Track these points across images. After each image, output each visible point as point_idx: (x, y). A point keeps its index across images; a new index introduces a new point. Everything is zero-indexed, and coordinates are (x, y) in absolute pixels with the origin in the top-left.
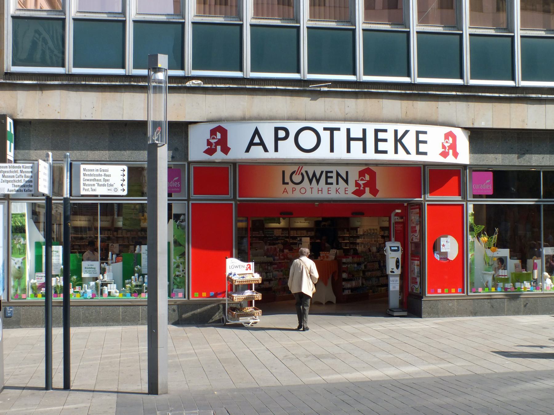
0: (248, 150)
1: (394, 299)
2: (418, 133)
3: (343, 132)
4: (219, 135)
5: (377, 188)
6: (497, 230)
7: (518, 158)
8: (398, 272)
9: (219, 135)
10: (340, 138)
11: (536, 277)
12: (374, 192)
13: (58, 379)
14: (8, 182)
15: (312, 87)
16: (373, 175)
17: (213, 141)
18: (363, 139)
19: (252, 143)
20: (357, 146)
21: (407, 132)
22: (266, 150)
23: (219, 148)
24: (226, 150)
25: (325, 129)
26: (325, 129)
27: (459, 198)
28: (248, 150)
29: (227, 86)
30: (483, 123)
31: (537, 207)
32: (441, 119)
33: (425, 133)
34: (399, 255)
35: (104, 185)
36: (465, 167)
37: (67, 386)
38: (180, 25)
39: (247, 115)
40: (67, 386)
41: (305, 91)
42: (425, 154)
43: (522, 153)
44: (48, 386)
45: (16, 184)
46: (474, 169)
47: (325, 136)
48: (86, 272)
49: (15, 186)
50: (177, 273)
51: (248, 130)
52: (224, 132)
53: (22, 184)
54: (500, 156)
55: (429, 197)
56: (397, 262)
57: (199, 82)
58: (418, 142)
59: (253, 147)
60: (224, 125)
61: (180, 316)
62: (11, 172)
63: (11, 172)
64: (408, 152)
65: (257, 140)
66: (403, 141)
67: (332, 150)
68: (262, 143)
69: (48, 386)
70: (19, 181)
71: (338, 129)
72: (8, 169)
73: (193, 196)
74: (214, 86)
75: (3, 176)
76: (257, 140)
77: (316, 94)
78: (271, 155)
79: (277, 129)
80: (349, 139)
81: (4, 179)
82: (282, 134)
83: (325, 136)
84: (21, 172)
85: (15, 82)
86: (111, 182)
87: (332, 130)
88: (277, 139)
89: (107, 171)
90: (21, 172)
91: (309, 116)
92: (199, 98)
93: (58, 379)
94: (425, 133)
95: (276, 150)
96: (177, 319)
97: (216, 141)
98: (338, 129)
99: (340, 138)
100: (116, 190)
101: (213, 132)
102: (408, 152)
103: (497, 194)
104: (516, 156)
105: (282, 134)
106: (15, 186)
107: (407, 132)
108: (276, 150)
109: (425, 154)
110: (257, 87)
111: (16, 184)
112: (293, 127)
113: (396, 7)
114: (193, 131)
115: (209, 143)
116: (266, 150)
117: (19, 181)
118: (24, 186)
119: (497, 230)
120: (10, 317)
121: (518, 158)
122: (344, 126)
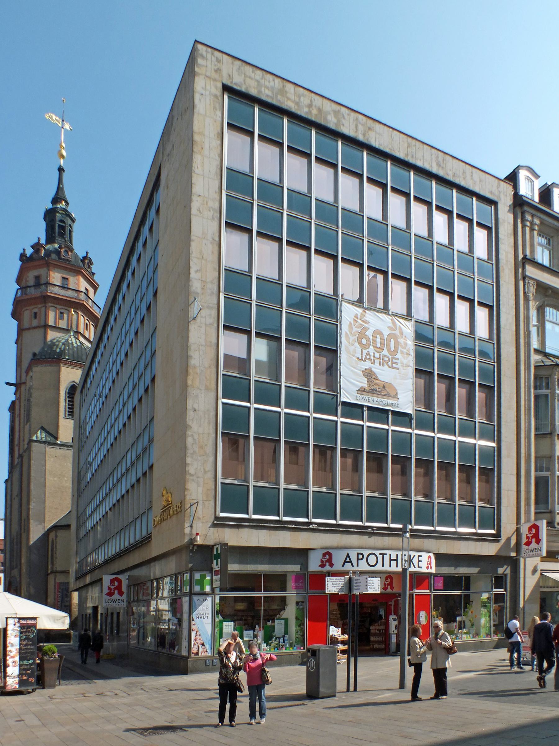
0: (343, 566)
1: (393, 647)
2: (419, 556)
3: (388, 556)
4: (328, 557)
5: (394, 586)
6: (440, 608)
7: (455, 569)
8: (396, 632)
9: (328, 557)
10: (387, 558)
11: (456, 633)
12: (392, 588)
13: (352, 688)
14: (334, 587)
15: (369, 530)
16: (391, 578)
17: (324, 560)
18: (397, 560)
19: (345, 562)
20: (394, 563)
21: (414, 556)
22: (353, 566)
23: (327, 564)
24: (331, 565)
25: (380, 554)
26: (380, 554)
27: (428, 591)
28: (343, 566)
29: (331, 529)
30: (443, 551)
31: (460, 595)
32: (425, 549)
33: (421, 556)
34: (396, 622)
35: (372, 588)
36: (431, 574)
37: (355, 689)
38: (306, 492)
39: (340, 545)
40: (355, 689)
41: (366, 532)
42: (421, 567)
43: (456, 566)
44: (348, 690)
45: (338, 588)
46: (436, 575)
47: (380, 557)
48: (247, 637)
49: (337, 589)
50: (297, 636)
51: (344, 554)
52: (330, 555)
53: (340, 588)
54: (447, 568)
55: (416, 591)
56: (396, 626)
57: (316, 526)
58: (419, 561)
59: (346, 564)
60: (330, 551)
61: (302, 660)
62: (336, 582)
63: (336, 582)
64: (415, 567)
65: (348, 560)
66: (413, 561)
67: (383, 566)
68: (351, 562)
69: (348, 690)
70: (339, 586)
71: (386, 554)
72: (334, 580)
73: (309, 591)
74: (325, 528)
75: (333, 584)
76: (348, 560)
77: (371, 534)
78: (355, 568)
79: (358, 554)
80: (391, 560)
81: (333, 585)
82: (360, 557)
83: (380, 557)
84: (340, 581)
85: (225, 523)
86: (374, 587)
87: (383, 555)
88: (358, 559)
89: (373, 581)
90: (340, 581)
91: (367, 547)
92: (317, 535)
93: (352, 688)
94: (421, 556)
95: (358, 566)
96: (301, 662)
97: (326, 560)
98: (386, 554)
99: (387, 558)
100: (376, 590)
101: (324, 555)
102: (415, 567)
103: (445, 589)
104: (453, 568)
105: (360, 557)
106: (337, 589)
107: (414, 556)
108: (358, 566)
109: (421, 567)
110: (345, 529)
111: (338, 588)
112: (366, 553)
113: (275, 463)
114: (312, 555)
115: (322, 561)
116: (353, 566)
117: (339, 586)
118: (341, 589)
119: (440, 608)
120: (215, 665)
121: (455, 569)
122: (388, 552)
